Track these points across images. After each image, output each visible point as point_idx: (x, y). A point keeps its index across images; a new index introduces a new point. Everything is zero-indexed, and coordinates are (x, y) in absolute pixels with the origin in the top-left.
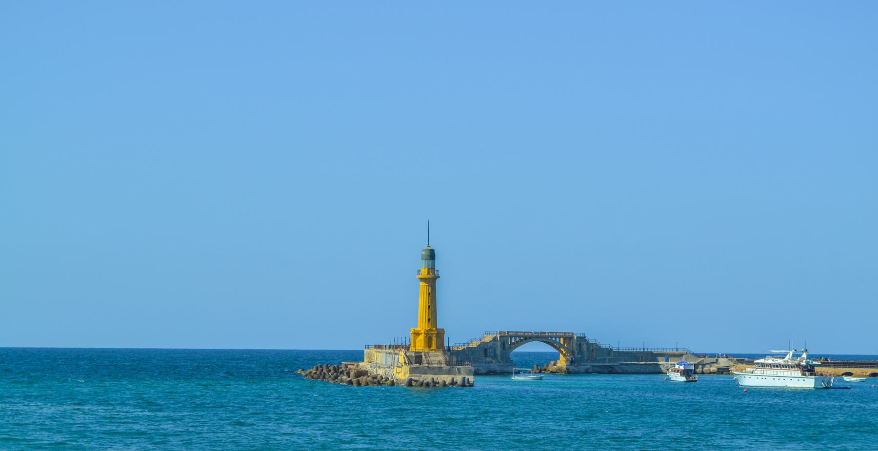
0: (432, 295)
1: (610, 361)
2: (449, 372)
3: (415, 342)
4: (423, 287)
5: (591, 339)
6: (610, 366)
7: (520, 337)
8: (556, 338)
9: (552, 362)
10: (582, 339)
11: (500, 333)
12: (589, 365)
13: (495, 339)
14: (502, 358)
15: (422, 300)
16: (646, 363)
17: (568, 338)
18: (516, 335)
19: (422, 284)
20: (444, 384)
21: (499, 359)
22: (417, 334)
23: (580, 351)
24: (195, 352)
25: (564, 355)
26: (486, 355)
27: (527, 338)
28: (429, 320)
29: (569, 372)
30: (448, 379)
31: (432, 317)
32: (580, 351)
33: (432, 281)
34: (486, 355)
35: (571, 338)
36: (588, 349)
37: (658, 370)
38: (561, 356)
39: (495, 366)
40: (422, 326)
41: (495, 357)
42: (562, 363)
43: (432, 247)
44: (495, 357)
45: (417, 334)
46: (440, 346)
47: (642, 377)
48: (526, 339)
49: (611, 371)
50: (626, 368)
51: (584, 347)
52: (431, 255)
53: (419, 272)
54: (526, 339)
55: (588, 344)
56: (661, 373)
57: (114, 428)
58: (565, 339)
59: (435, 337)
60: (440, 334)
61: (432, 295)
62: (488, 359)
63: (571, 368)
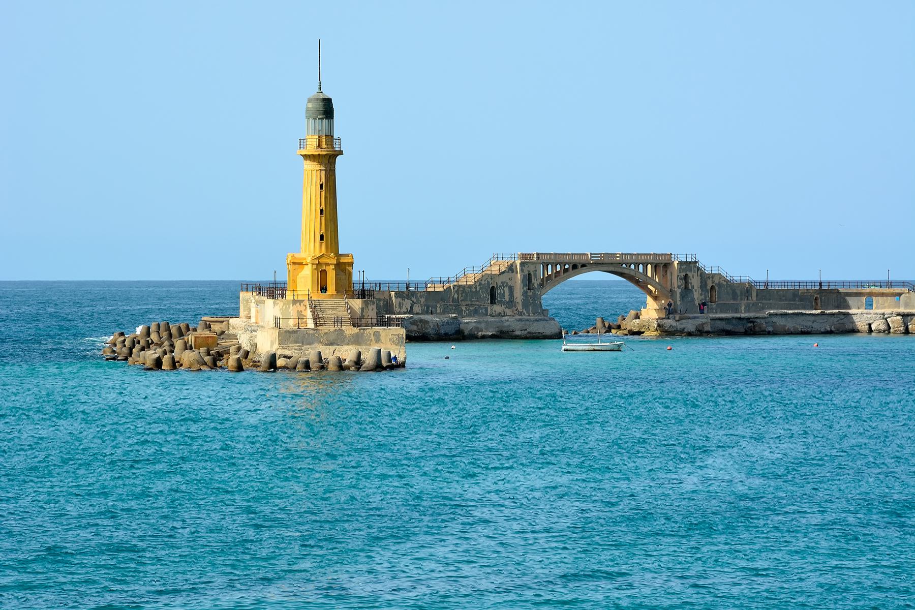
0: (329, 187)
1: (748, 309)
2: (356, 340)
3: (294, 281)
4: (312, 172)
5: (709, 264)
6: (748, 320)
7: (563, 264)
8: (637, 265)
9: (633, 312)
10: (690, 266)
11: (524, 256)
12: (704, 319)
13: (511, 268)
14: (525, 305)
15: (309, 198)
16: (820, 310)
17: (662, 265)
18: (546, 260)
19: (310, 166)
20: (341, 367)
21: (520, 308)
22: (298, 264)
23: (687, 289)
24: (42, 282)
25: (655, 298)
26: (493, 300)
27: (578, 265)
28: (322, 238)
29: (666, 332)
30: (348, 353)
31: (329, 235)
32: (687, 289)
33: (328, 160)
34: (493, 300)
35: (667, 265)
36: (703, 285)
37: (848, 326)
38: (649, 300)
39: (510, 322)
40: (309, 248)
41: (499, 308)
42: (651, 312)
43: (327, 94)
44: (511, 303)
45: (298, 264)
46: (346, 287)
47: (812, 342)
48: (575, 267)
49: (752, 329)
50: (781, 322)
51: (695, 282)
52: (327, 110)
53: (302, 143)
54: (575, 267)
55: (704, 277)
56: (854, 331)
57: (810, 324)
58: (656, 267)
59: (336, 274)
60: (343, 268)
61: (329, 187)
62: (498, 308)
63: (669, 323)
